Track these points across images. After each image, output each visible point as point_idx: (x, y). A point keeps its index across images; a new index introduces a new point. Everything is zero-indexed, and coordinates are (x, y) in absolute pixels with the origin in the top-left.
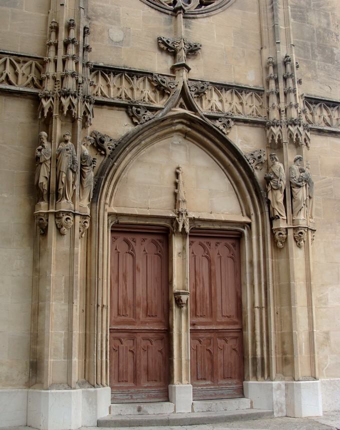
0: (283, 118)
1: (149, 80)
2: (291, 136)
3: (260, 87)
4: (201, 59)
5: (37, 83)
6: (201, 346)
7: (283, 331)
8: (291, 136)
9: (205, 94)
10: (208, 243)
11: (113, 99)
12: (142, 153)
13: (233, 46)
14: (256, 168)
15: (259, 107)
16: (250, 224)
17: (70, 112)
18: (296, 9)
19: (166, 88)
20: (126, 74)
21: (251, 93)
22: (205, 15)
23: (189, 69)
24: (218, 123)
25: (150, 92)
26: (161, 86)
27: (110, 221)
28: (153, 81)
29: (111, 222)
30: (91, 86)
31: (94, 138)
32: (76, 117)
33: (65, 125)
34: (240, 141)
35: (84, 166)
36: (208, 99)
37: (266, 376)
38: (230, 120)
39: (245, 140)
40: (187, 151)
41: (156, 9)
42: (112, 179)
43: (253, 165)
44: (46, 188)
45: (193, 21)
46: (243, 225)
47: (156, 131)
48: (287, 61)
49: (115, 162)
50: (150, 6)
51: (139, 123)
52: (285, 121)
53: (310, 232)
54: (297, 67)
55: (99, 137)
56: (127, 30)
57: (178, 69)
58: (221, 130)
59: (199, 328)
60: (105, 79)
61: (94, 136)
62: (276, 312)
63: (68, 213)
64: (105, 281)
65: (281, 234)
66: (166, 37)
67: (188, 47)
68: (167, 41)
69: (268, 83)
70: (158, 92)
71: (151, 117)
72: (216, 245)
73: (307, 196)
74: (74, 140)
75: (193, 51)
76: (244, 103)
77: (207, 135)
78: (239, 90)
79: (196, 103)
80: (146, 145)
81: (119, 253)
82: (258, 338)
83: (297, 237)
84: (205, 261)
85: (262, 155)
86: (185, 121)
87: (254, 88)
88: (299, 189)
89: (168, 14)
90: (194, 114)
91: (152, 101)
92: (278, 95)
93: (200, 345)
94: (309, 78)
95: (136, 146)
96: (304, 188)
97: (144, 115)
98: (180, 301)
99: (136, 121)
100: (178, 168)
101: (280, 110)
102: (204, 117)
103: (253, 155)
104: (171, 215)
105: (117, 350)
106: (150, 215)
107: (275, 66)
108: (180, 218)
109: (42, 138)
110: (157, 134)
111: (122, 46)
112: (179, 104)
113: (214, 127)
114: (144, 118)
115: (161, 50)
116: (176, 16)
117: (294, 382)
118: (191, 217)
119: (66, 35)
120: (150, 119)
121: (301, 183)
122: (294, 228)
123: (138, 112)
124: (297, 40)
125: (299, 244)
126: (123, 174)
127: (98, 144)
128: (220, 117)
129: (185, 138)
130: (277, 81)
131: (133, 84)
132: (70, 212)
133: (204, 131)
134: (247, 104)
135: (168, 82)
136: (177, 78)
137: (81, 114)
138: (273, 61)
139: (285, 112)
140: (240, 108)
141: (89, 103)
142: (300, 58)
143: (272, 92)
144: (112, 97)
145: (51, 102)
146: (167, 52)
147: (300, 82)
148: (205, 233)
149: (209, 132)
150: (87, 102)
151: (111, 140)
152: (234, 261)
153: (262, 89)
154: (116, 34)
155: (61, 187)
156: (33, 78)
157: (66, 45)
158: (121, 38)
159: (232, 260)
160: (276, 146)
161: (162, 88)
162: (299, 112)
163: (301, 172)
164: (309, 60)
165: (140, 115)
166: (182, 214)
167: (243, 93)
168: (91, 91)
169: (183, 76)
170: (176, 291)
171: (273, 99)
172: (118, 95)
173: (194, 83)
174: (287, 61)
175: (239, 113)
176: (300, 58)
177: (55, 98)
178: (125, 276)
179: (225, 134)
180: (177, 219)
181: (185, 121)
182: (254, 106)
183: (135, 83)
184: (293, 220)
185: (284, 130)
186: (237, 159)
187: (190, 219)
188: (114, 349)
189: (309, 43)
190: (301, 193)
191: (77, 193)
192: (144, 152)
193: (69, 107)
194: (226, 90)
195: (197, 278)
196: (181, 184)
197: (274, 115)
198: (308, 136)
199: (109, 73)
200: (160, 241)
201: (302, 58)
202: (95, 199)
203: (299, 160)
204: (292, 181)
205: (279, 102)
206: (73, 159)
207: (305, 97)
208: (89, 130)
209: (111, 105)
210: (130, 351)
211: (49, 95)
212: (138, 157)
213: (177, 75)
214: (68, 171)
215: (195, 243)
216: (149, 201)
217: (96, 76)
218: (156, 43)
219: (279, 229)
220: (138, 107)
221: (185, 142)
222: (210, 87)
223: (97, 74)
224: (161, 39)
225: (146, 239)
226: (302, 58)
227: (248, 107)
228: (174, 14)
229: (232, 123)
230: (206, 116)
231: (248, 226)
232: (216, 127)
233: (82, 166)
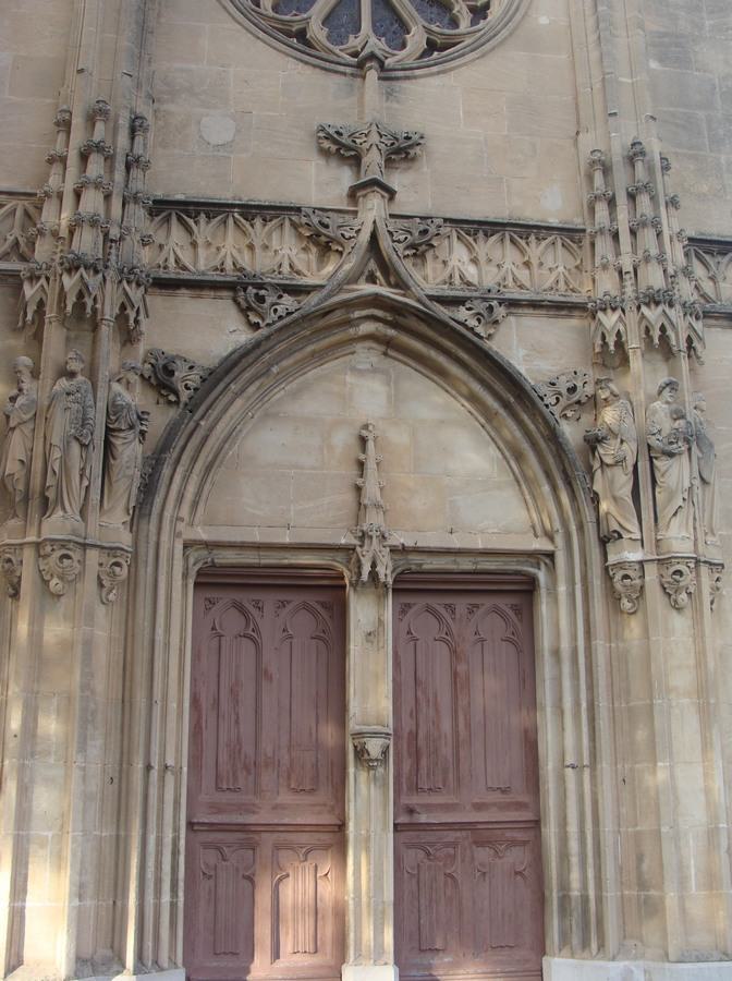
0: (629, 290)
1: (294, 226)
2: (647, 330)
3: (577, 222)
4: (425, 169)
5: (26, 250)
6: (430, 867)
7: (639, 828)
8: (647, 330)
9: (432, 246)
10: (449, 607)
11: (203, 274)
12: (278, 396)
13: (506, 133)
14: (565, 416)
15: (574, 270)
16: (551, 556)
17: (664, 337)
18: (666, 40)
19: (332, 240)
20: (236, 215)
21: (553, 237)
22: (435, 69)
23: (391, 193)
24: (462, 314)
25: (295, 251)
26: (319, 235)
27: (192, 560)
28: (301, 225)
29: (194, 564)
30: (144, 245)
31: (152, 365)
32: (99, 318)
33: (76, 338)
34: (522, 352)
35: (114, 430)
36: (441, 258)
37: (594, 945)
38: (494, 303)
39: (536, 350)
40: (389, 385)
41: (315, 66)
42: (194, 459)
43: (557, 410)
44: (21, 487)
45: (405, 84)
46: (534, 556)
47: (308, 340)
48: (636, 153)
49: (202, 418)
50: (302, 61)
51: (262, 325)
52: (633, 297)
53: (704, 569)
54: (666, 168)
55: (161, 362)
56: (251, 115)
57: (364, 192)
58: (471, 330)
59: (423, 818)
60: (187, 229)
61: (153, 361)
62: (620, 779)
63: (63, 544)
64: (173, 705)
65: (626, 577)
66: (335, 122)
67: (389, 143)
68: (337, 133)
69: (592, 210)
70: (314, 249)
71: (291, 309)
72: (471, 612)
73: (692, 478)
74: (92, 374)
75: (402, 151)
76: (535, 262)
77: (440, 339)
78: (521, 231)
79: (406, 267)
80: (286, 376)
81: (221, 636)
82: (574, 846)
83: (669, 583)
84: (442, 651)
85: (579, 384)
86: (379, 313)
87: (560, 225)
88: (671, 461)
89: (344, 74)
90: (404, 295)
91: (298, 273)
92: (616, 236)
93: (428, 863)
94: (705, 195)
95: (256, 379)
96: (685, 457)
97: (278, 304)
98: (366, 755)
99: (254, 319)
100: (366, 427)
101: (620, 273)
102: (428, 302)
103: (553, 384)
104: (343, 541)
105: (211, 876)
106: (290, 544)
107: (607, 170)
108: (365, 548)
109: (20, 372)
110: (310, 348)
111: (232, 152)
112: (366, 273)
113: (453, 323)
114: (276, 310)
115: (325, 153)
116: (364, 77)
117: (667, 965)
118: (394, 543)
119: (109, 138)
120: (289, 314)
121: (675, 446)
122: (659, 560)
123: (261, 299)
124: (671, 109)
125: (676, 601)
126: (227, 446)
127: (161, 378)
128: (469, 298)
129: (385, 354)
130: (612, 203)
131: (253, 234)
132: (69, 541)
133: (430, 333)
134: (541, 264)
135: (336, 225)
136: (359, 214)
137: (112, 309)
138: (603, 158)
139: (632, 275)
140: (523, 275)
141: (134, 285)
142: (678, 150)
143: (601, 231)
144: (203, 268)
145: (42, 286)
146: (343, 159)
147: (673, 203)
148: (423, 583)
149: (441, 335)
150: (129, 282)
151: (191, 368)
152: (519, 651)
153: (582, 227)
154: (218, 128)
155: (50, 481)
156: (17, 239)
157: (84, 157)
158: (227, 136)
159: (512, 649)
160: (613, 356)
161: (323, 239)
162: (671, 271)
163: (675, 420)
164: (702, 153)
165: (265, 305)
166: (371, 537)
167: (532, 238)
168: (146, 256)
169: (373, 209)
170: (357, 727)
171: (604, 246)
172: (217, 263)
173: (401, 223)
174: (636, 153)
175: (521, 287)
176: (678, 150)
177: (52, 278)
178: (234, 693)
179: (481, 338)
180: (358, 549)
181: (379, 313)
182: (561, 269)
183: (201, 230)
184: (658, 541)
185: (632, 317)
186: (515, 398)
187: (393, 550)
188: (204, 874)
189: (701, 114)
190: (676, 473)
191: (95, 495)
192: (282, 392)
193: (80, 295)
194: (487, 235)
195: (419, 693)
196: (371, 466)
197: (43, 251)
198: (695, 331)
199: (195, 217)
200: (323, 605)
201: (685, 151)
202: (141, 509)
203: (668, 389)
204: (653, 441)
205: (618, 254)
206: (84, 415)
207: (690, 239)
208: (142, 348)
209: (197, 286)
210: (244, 877)
211: (37, 273)
212: (266, 405)
213: (360, 208)
214: (68, 443)
215: (414, 609)
216: (292, 508)
217: (165, 225)
218: (315, 138)
219: (621, 565)
220: (260, 286)
221: (387, 363)
222: (445, 230)
223: (167, 219)
224: (323, 130)
225: (288, 602)
226: (685, 151)
227: (545, 271)
228: (359, 73)
229: (500, 311)
230: (432, 298)
231: (547, 561)
232: (459, 323)
233: (109, 431)
